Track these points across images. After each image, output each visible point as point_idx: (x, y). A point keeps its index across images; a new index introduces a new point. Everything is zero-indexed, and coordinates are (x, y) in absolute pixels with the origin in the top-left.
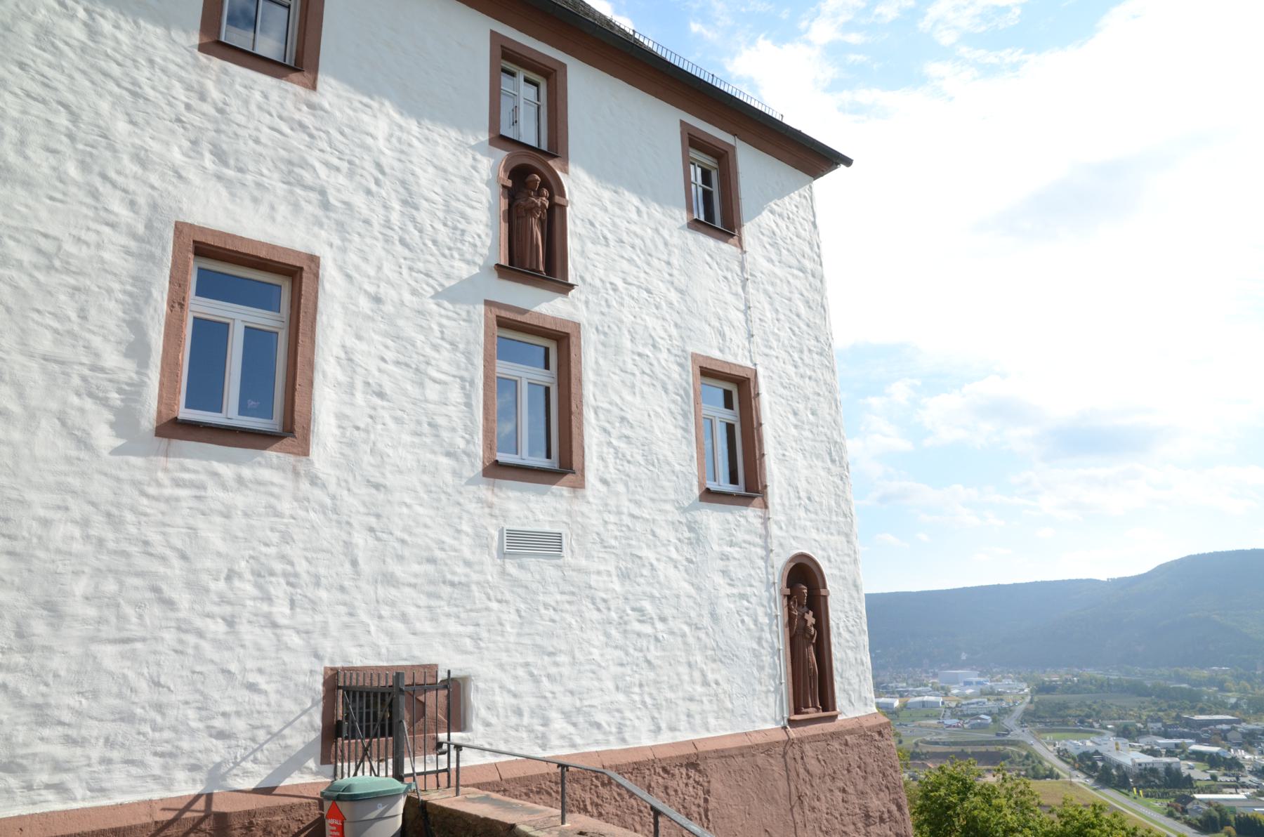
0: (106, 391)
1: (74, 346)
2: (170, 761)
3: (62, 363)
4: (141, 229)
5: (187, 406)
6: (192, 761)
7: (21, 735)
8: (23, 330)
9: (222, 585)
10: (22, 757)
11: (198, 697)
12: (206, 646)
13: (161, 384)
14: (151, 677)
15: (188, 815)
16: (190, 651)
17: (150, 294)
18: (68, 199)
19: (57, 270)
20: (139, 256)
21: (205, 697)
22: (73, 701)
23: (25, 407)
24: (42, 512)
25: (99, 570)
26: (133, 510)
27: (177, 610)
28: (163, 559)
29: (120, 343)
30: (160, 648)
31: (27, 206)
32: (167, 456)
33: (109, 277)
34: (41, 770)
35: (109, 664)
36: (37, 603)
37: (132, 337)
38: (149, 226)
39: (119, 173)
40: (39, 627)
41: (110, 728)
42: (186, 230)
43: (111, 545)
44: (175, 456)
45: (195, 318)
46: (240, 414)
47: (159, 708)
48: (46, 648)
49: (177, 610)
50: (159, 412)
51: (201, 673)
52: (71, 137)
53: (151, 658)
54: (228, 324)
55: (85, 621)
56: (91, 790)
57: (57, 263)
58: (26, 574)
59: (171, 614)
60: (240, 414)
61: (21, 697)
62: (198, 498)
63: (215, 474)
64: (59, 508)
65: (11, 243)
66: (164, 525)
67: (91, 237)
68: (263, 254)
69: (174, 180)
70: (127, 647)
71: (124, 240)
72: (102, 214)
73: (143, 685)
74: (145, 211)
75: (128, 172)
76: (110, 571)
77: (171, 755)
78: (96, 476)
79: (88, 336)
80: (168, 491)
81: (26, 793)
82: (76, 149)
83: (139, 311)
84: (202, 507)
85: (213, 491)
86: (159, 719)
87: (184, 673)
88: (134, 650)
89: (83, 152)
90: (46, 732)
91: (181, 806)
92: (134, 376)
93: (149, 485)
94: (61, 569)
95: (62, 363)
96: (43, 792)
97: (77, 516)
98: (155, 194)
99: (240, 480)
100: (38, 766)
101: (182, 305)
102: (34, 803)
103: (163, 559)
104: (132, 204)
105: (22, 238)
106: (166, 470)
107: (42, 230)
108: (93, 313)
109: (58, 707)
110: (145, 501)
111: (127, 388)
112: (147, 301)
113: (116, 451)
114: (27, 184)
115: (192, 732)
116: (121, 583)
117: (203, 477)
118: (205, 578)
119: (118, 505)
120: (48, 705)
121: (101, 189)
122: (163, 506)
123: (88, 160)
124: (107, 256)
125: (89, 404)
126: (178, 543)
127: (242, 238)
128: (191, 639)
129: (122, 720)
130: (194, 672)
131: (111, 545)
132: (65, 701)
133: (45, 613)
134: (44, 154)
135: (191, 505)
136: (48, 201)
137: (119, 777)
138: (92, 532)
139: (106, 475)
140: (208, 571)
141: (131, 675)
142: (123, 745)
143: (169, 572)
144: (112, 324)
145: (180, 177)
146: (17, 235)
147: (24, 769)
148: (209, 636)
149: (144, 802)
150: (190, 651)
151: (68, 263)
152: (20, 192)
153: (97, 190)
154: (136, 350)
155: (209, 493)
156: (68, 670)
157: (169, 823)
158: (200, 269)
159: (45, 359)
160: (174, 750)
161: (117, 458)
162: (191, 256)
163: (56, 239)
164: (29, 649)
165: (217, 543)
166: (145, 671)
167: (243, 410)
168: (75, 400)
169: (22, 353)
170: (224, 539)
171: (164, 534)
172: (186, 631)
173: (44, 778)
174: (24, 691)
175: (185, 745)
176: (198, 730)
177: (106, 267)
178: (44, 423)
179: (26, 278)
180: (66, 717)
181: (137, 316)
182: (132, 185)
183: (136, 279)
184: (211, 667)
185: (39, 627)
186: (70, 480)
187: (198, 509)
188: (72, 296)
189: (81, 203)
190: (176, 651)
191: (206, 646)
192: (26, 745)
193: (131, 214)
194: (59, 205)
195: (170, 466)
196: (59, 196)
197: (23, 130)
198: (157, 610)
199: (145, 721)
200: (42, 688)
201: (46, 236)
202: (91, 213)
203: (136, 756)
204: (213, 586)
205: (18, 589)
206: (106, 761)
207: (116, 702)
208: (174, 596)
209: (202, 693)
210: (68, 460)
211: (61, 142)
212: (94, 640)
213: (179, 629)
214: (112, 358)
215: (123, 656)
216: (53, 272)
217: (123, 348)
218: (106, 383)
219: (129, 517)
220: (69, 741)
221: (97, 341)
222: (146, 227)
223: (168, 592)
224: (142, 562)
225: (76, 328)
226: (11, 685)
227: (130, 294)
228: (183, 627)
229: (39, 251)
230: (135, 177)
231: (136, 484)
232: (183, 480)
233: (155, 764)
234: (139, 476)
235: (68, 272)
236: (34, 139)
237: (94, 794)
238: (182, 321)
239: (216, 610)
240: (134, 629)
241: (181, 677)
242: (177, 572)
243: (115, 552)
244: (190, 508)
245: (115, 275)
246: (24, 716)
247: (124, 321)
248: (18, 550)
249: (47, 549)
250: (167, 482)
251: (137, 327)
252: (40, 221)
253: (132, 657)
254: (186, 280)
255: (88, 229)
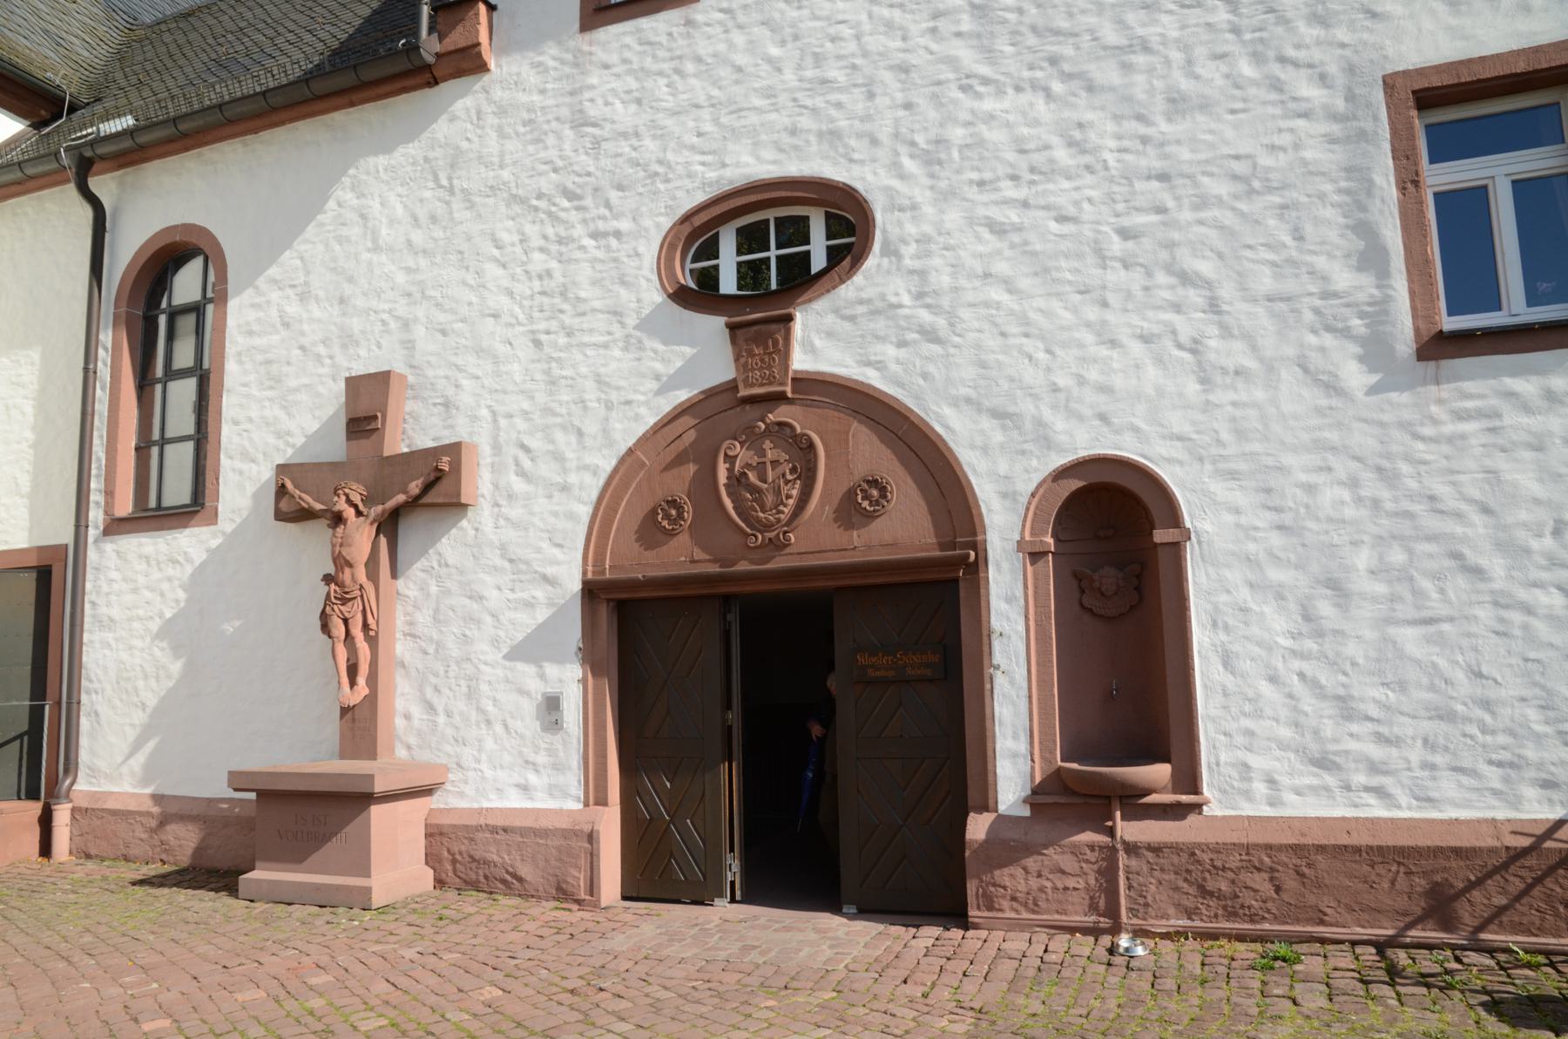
0: (1345, 320)
1: (1297, 276)
2: (1513, 773)
3: (1288, 299)
4: (1340, 104)
5: (1450, 314)
6: (1544, 776)
7: (1328, 729)
8: (1239, 274)
9: (1548, 542)
10: (1335, 753)
11: (1537, 691)
12: (1541, 628)
13: (1412, 293)
14: (1469, 666)
15: (1549, 844)
16: (1517, 632)
17: (1371, 182)
18: (1250, 105)
19: (1258, 193)
20: (1347, 140)
21: (1550, 692)
22: (1379, 693)
23: (1261, 360)
24: (1303, 477)
25: (1381, 538)
26: (1408, 458)
27: (1490, 580)
28: (1458, 516)
29: (1348, 256)
30: (1474, 629)
31: (1211, 132)
32: (1438, 383)
33: (1317, 179)
34: (1357, 770)
35: (1412, 649)
36: (1318, 582)
37: (1361, 244)
38: (1350, 97)
39: (1298, 47)
40: (1325, 609)
41: (1427, 726)
42: (1399, 82)
43: (1389, 506)
44: (1449, 381)
45: (1435, 194)
46: (1529, 305)
47: (1486, 704)
48: (1336, 632)
49: (1490, 580)
50: (1417, 330)
51: (1538, 661)
52: (1236, 30)
53: (1465, 642)
54: (1485, 187)
55: (1375, 599)
56: (1417, 799)
57: (1256, 184)
58: (1300, 549)
59: (1482, 586)
60: (1529, 305)
61: (1322, 687)
62: (1492, 430)
63: (1511, 395)
64: (1321, 469)
65: (1205, 180)
66: (1452, 472)
67: (1285, 139)
68: (1521, 67)
69: (1368, 23)
70: (1432, 629)
71: (1324, 127)
72: (1292, 105)
73: (1460, 676)
74: (1340, 80)
75: (1308, 41)
76: (1394, 537)
77: (1512, 765)
78: (1355, 425)
79: (1309, 258)
80: (1449, 428)
81: (1346, 794)
82: (1243, 42)
83: (1363, 208)
84: (1500, 441)
85: (1512, 418)
86: (1488, 718)
87: (1513, 661)
88: (1441, 633)
89: (1252, 41)
90: (1355, 728)
91: (1539, 832)
92: (1375, 292)
93: (1422, 424)
94: (1336, 540)
95: (1288, 299)
96: (1364, 795)
97: (1344, 477)
98: (1348, 52)
99: (1550, 396)
100: (1353, 765)
101: (1416, 183)
102: (1356, 806)
103: (1458, 516)
104: (1323, 79)
105: (1215, 170)
106: (1440, 402)
107: (1232, 152)
108: (1309, 229)
109: (1362, 700)
110: (1420, 446)
111: (1369, 309)
112: (1369, 194)
113: (1372, 390)
114: (1205, 106)
115: (1538, 738)
116: (1410, 551)
117: (1494, 402)
118: (1522, 535)
119: (1389, 456)
120: (1351, 697)
121: (1283, 76)
122: (1445, 449)
123: (1260, 48)
124: (1308, 154)
125: (1328, 340)
126: (1476, 494)
127: (1482, 59)
128: (1517, 617)
129: (1441, 718)
130: (1526, 660)
131: (1389, 506)
132: (1370, 693)
133: (1329, 592)
134: (1212, 65)
135: (1483, 441)
136: (1230, 117)
137: (1447, 786)
138: (1363, 493)
139: (1366, 421)
140: (1525, 525)
141: (1442, 663)
142: (1446, 749)
143: (1469, 532)
144: (1333, 235)
145: (1374, 15)
146: (1209, 169)
147: (1338, 767)
148: (1541, 611)
149: (1486, 820)
150: (1517, 632)
151: (1267, 180)
152: (1201, 118)
153: (1278, 79)
154: (1371, 259)
155: (1508, 420)
156: (1367, 657)
157: (1525, 852)
158: (1429, 128)
159: (1270, 300)
160: (1516, 760)
161: (1374, 398)
162: (1414, 113)
163: (1248, 157)
164: (1319, 634)
165: (1531, 485)
166: (1460, 658)
167: (1533, 299)
168: (1312, 339)
169: (1245, 300)
170: (1541, 480)
171: (1454, 484)
172: (1507, 607)
173: (1360, 779)
174: (1323, 682)
175: (1530, 753)
176: (1546, 736)
177: (1311, 168)
178: (1284, 374)
179: (1229, 214)
180: (1374, 711)
181: (1362, 215)
182: (1317, 55)
183: (1349, 170)
184: (1551, 653)
185: (1325, 609)
186: (1327, 434)
187: (1494, 445)
188: (1281, 217)
189: (1264, 103)
190: (1497, 633)
191: (1541, 628)
192: (1336, 741)
193: (1325, 92)
194: (1241, 116)
195: (1444, 395)
196: (1239, 105)
197: (1186, 48)
198: (1461, 581)
199: (1470, 720)
200: (1341, 678)
201: (1237, 157)
202: (1278, 111)
203: (1466, 764)
204: (1535, 544)
205: (1297, 567)
206: (1428, 766)
207: (1429, 696)
208: (1483, 562)
209: (1543, 688)
210: (1319, 411)
211: (1227, 41)
212: (1389, 621)
213: (1496, 604)
214: (1343, 278)
215: (1428, 640)
216: (1254, 197)
217: (1353, 261)
218: (1343, 310)
219: (1405, 468)
220: (1381, 739)
221: (1321, 262)
222: (1347, 100)
223: (1472, 557)
224: (1432, 523)
225: (1294, 253)
226: (1309, 673)
227: (1348, 192)
228: (1500, 602)
229: (1235, 177)
230: (1318, 43)
231: (1404, 426)
232: (1466, 410)
233: (1493, 776)
234: (1407, 415)
235: (1270, 190)
236: (1200, 52)
237: (1424, 804)
238: (1421, 203)
239: (1545, 576)
240: (1436, 607)
241: (1510, 666)
242: (1481, 530)
243: (1396, 514)
244: (1484, 446)
245: (1323, 174)
246: (1328, 708)
247: (1347, 227)
248: (1287, 523)
249: (1318, 519)
250: (1444, 417)
251: (1365, 230)
252: (1228, 143)
253: (1440, 641)
254: (1414, 148)
255: (1280, 130)
